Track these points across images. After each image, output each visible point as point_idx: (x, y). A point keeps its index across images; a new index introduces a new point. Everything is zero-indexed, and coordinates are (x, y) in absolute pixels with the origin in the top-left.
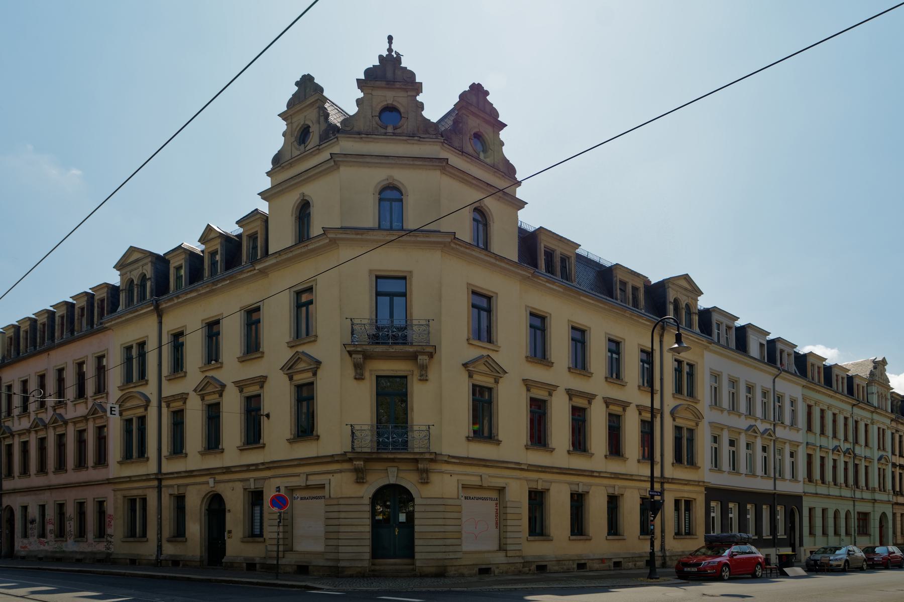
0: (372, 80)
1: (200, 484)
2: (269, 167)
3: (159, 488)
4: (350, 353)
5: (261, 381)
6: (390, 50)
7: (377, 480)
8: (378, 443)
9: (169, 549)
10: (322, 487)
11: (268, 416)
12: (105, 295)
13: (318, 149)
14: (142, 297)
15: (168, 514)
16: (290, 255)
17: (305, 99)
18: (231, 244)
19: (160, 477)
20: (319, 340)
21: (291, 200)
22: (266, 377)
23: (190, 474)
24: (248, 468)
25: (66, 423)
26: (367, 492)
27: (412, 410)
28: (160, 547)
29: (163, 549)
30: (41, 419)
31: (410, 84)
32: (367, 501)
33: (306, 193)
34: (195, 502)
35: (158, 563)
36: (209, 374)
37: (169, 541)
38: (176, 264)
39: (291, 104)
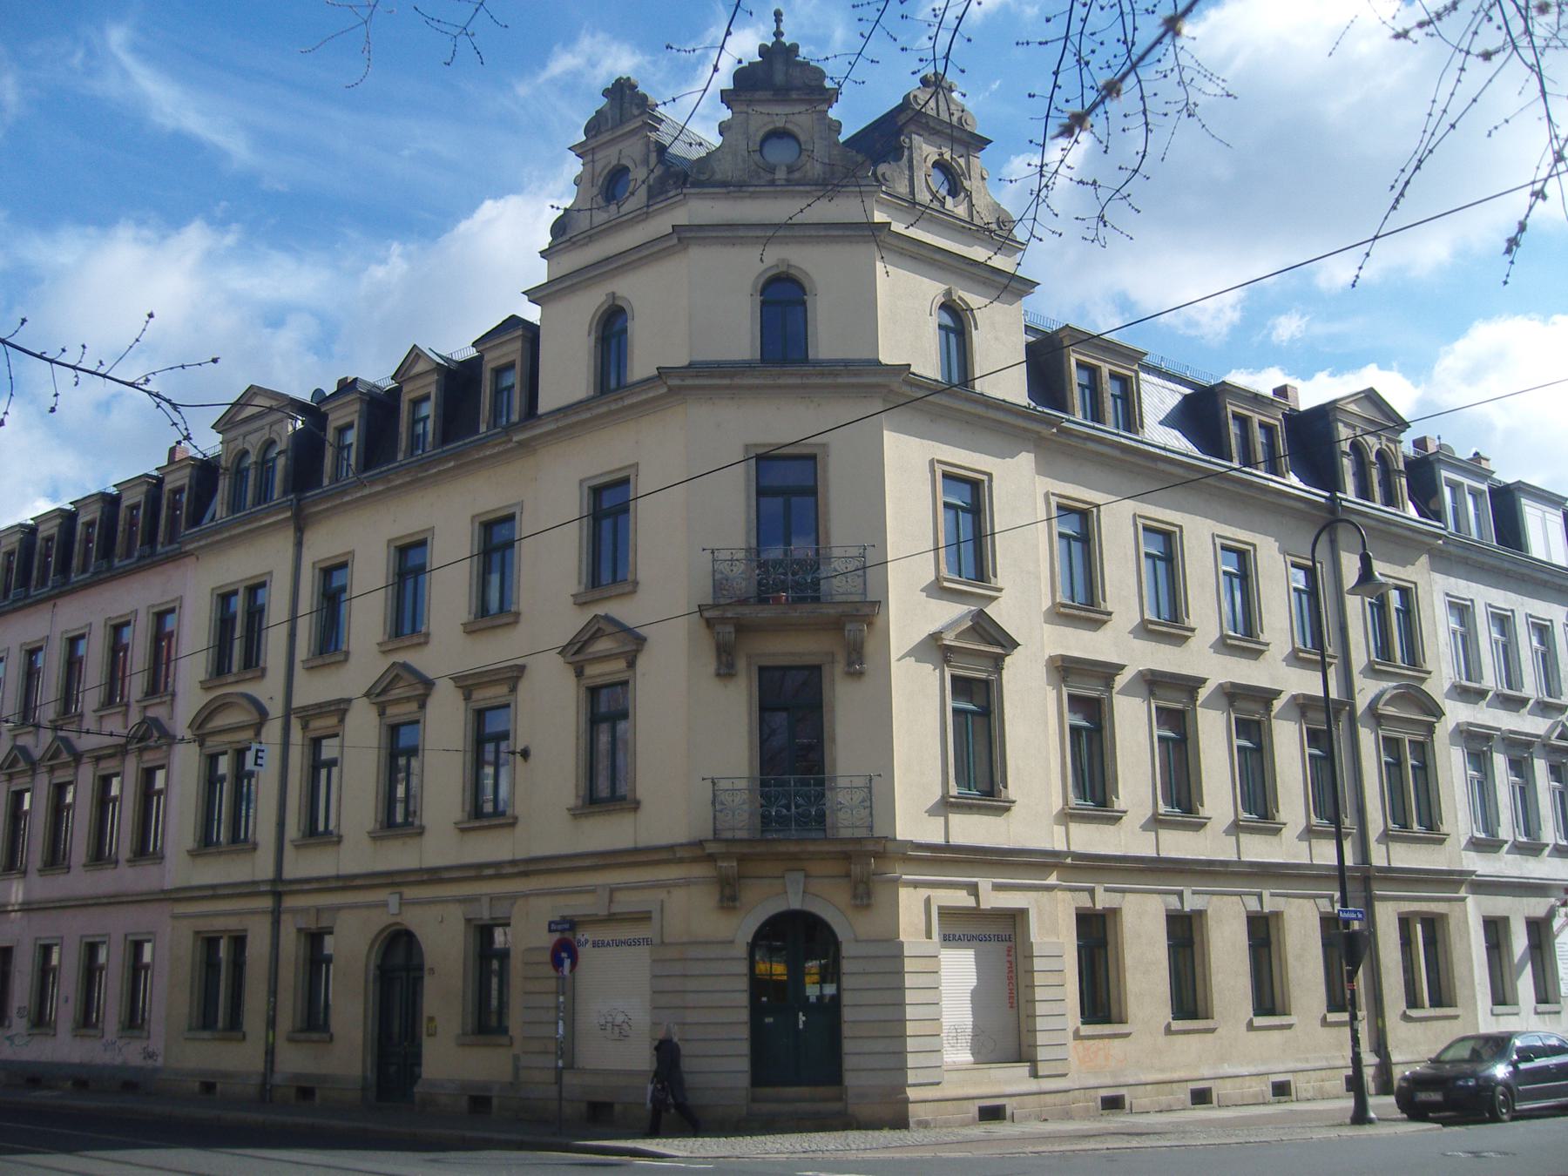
0: (748, 85)
1: (369, 906)
2: (545, 240)
3: (276, 915)
4: (709, 623)
5: (513, 675)
6: (778, 34)
7: (763, 904)
8: (766, 820)
9: (295, 1061)
10: (643, 917)
11: (525, 754)
12: (186, 481)
13: (644, 215)
14: (263, 494)
15: (290, 975)
16: (587, 415)
17: (622, 122)
18: (459, 380)
19: (280, 888)
20: (641, 588)
21: (590, 302)
22: (521, 669)
23: (346, 883)
24: (477, 872)
25: (77, 757)
26: (745, 926)
27: (833, 740)
28: (270, 1053)
29: (279, 1058)
30: (24, 750)
31: (814, 90)
32: (741, 950)
33: (619, 293)
34: (353, 943)
35: (266, 1092)
36: (400, 657)
37: (291, 1040)
38: (341, 422)
39: (593, 128)
